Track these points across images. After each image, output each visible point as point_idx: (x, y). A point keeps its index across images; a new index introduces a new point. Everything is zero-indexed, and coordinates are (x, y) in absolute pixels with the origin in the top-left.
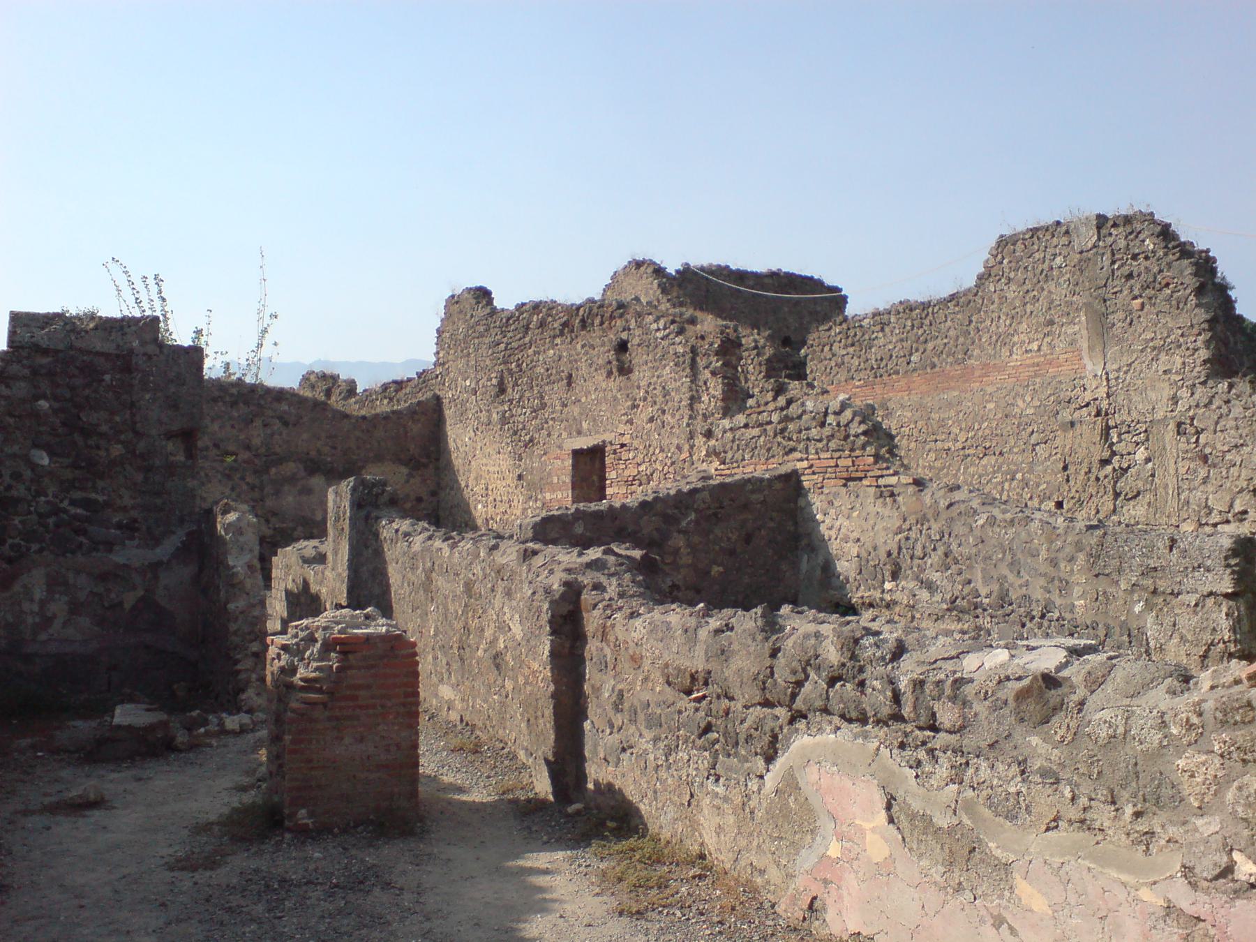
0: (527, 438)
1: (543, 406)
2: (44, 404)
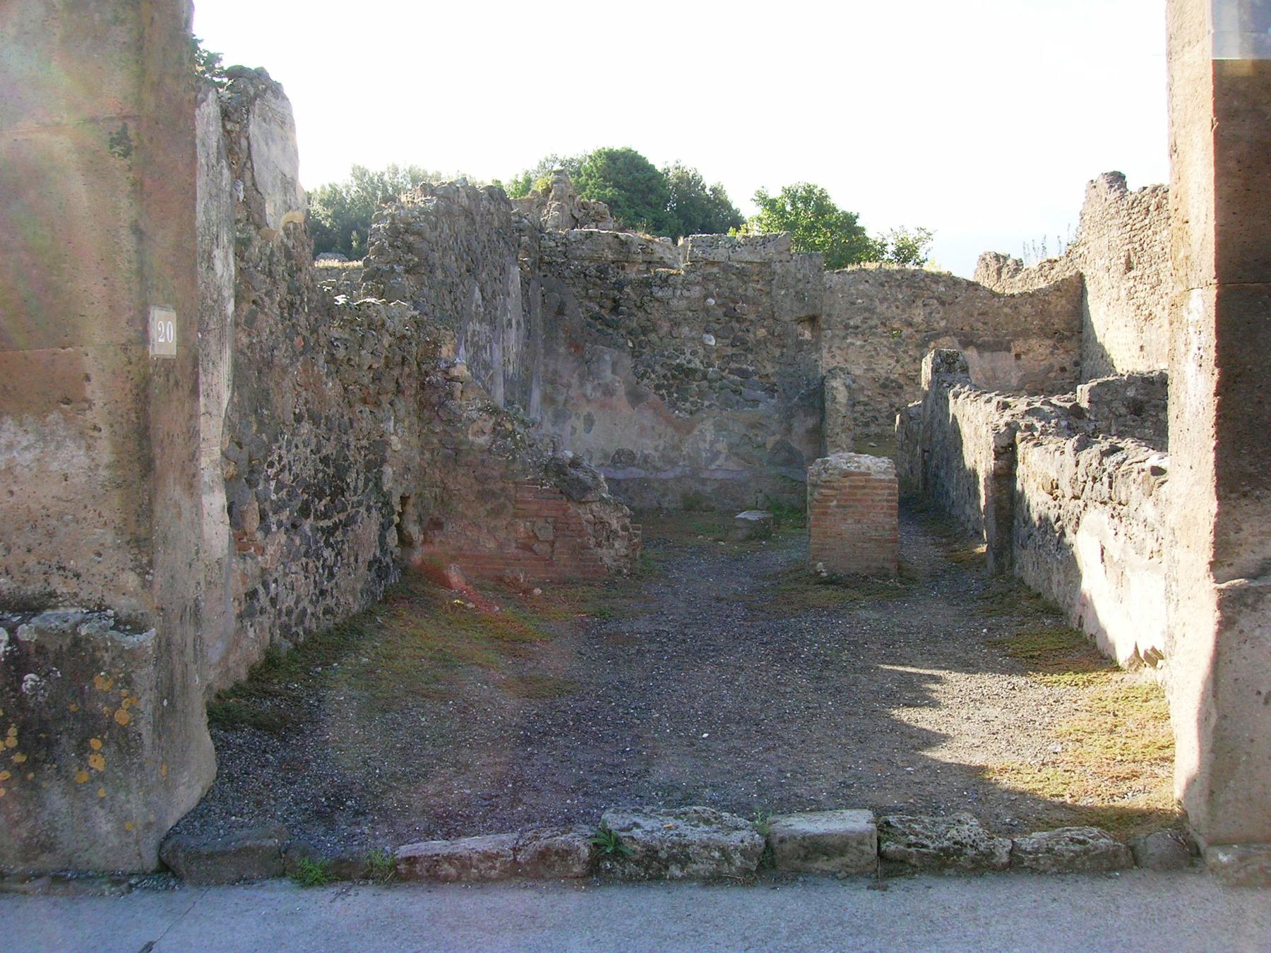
0: (1147, 313)
1: (1160, 282)
2: (711, 301)
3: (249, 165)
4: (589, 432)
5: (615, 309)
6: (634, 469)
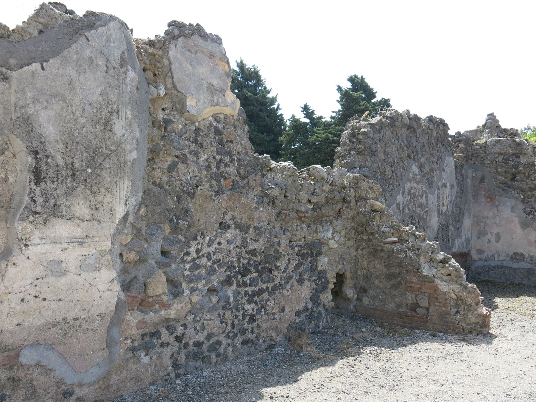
3: (170, 74)
4: (498, 242)
5: (513, 179)
6: (523, 263)
